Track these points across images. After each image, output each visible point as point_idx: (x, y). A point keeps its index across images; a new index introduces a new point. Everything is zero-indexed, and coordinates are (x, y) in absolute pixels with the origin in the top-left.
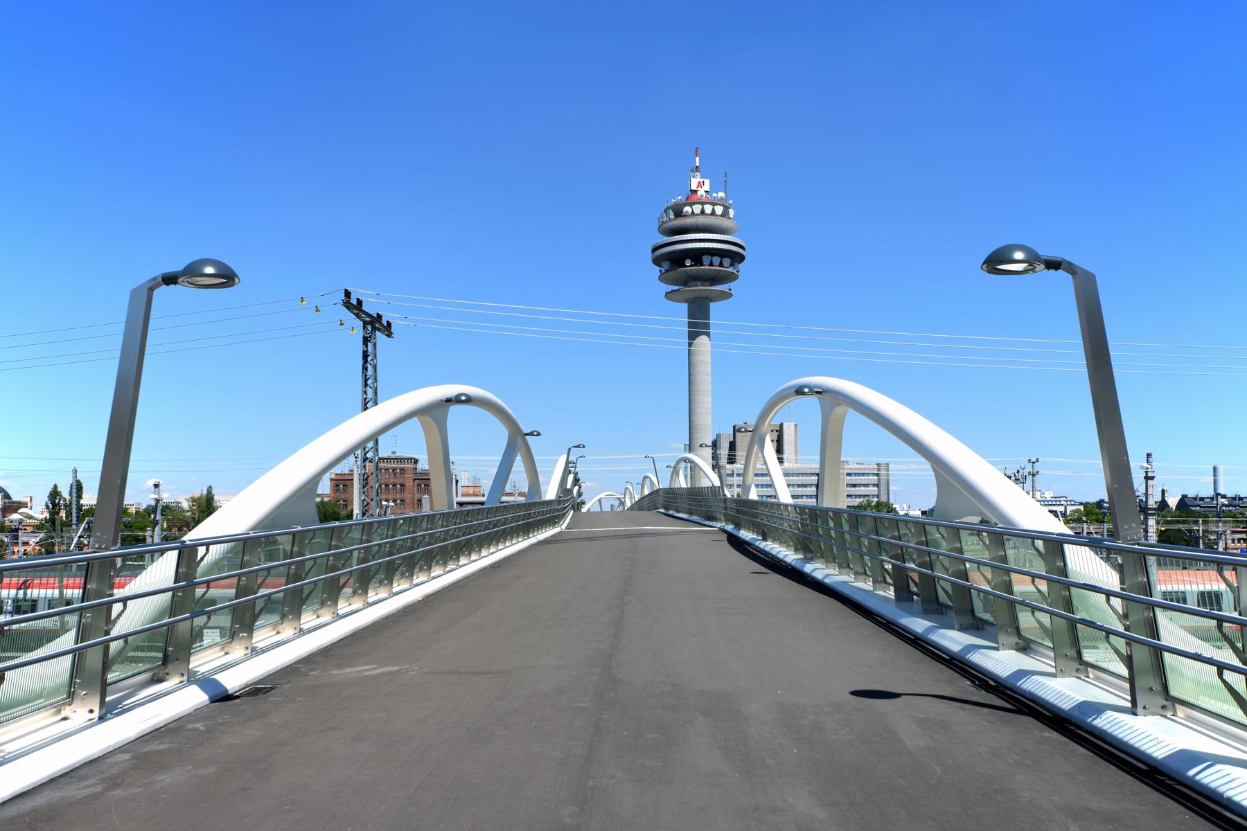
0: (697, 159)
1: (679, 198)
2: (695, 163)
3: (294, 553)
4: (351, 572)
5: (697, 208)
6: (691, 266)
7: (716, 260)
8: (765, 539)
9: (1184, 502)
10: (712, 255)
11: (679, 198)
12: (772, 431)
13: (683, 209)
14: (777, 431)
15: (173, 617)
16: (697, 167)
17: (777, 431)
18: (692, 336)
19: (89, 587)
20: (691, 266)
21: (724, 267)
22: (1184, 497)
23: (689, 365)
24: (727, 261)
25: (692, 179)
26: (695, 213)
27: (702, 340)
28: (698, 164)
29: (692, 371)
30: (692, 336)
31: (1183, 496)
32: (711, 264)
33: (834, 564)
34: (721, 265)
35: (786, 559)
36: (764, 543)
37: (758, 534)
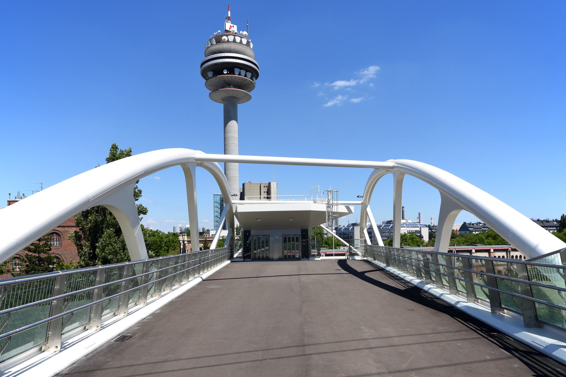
0: (229, 12)
1: (219, 31)
2: (228, 15)
3: (144, 271)
4: (153, 283)
5: (231, 38)
6: (227, 74)
7: (243, 72)
8: (375, 259)
9: (160, 231)
10: (241, 69)
11: (219, 31)
12: (264, 187)
13: (222, 38)
14: (267, 187)
15: (51, 316)
16: (229, 17)
17: (267, 187)
18: (227, 120)
19: (56, 288)
20: (227, 74)
21: (247, 77)
22: (465, 223)
23: (224, 139)
24: (249, 75)
25: (226, 23)
26: (230, 40)
27: (233, 124)
28: (229, 15)
29: (226, 143)
30: (227, 120)
31: (464, 223)
32: (239, 74)
33: (397, 267)
34: (245, 76)
35: (380, 266)
36: (375, 261)
37: (372, 258)
